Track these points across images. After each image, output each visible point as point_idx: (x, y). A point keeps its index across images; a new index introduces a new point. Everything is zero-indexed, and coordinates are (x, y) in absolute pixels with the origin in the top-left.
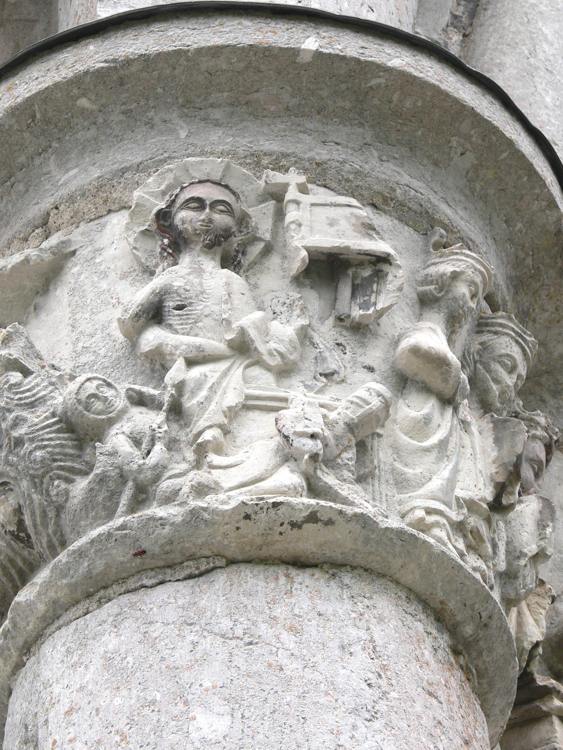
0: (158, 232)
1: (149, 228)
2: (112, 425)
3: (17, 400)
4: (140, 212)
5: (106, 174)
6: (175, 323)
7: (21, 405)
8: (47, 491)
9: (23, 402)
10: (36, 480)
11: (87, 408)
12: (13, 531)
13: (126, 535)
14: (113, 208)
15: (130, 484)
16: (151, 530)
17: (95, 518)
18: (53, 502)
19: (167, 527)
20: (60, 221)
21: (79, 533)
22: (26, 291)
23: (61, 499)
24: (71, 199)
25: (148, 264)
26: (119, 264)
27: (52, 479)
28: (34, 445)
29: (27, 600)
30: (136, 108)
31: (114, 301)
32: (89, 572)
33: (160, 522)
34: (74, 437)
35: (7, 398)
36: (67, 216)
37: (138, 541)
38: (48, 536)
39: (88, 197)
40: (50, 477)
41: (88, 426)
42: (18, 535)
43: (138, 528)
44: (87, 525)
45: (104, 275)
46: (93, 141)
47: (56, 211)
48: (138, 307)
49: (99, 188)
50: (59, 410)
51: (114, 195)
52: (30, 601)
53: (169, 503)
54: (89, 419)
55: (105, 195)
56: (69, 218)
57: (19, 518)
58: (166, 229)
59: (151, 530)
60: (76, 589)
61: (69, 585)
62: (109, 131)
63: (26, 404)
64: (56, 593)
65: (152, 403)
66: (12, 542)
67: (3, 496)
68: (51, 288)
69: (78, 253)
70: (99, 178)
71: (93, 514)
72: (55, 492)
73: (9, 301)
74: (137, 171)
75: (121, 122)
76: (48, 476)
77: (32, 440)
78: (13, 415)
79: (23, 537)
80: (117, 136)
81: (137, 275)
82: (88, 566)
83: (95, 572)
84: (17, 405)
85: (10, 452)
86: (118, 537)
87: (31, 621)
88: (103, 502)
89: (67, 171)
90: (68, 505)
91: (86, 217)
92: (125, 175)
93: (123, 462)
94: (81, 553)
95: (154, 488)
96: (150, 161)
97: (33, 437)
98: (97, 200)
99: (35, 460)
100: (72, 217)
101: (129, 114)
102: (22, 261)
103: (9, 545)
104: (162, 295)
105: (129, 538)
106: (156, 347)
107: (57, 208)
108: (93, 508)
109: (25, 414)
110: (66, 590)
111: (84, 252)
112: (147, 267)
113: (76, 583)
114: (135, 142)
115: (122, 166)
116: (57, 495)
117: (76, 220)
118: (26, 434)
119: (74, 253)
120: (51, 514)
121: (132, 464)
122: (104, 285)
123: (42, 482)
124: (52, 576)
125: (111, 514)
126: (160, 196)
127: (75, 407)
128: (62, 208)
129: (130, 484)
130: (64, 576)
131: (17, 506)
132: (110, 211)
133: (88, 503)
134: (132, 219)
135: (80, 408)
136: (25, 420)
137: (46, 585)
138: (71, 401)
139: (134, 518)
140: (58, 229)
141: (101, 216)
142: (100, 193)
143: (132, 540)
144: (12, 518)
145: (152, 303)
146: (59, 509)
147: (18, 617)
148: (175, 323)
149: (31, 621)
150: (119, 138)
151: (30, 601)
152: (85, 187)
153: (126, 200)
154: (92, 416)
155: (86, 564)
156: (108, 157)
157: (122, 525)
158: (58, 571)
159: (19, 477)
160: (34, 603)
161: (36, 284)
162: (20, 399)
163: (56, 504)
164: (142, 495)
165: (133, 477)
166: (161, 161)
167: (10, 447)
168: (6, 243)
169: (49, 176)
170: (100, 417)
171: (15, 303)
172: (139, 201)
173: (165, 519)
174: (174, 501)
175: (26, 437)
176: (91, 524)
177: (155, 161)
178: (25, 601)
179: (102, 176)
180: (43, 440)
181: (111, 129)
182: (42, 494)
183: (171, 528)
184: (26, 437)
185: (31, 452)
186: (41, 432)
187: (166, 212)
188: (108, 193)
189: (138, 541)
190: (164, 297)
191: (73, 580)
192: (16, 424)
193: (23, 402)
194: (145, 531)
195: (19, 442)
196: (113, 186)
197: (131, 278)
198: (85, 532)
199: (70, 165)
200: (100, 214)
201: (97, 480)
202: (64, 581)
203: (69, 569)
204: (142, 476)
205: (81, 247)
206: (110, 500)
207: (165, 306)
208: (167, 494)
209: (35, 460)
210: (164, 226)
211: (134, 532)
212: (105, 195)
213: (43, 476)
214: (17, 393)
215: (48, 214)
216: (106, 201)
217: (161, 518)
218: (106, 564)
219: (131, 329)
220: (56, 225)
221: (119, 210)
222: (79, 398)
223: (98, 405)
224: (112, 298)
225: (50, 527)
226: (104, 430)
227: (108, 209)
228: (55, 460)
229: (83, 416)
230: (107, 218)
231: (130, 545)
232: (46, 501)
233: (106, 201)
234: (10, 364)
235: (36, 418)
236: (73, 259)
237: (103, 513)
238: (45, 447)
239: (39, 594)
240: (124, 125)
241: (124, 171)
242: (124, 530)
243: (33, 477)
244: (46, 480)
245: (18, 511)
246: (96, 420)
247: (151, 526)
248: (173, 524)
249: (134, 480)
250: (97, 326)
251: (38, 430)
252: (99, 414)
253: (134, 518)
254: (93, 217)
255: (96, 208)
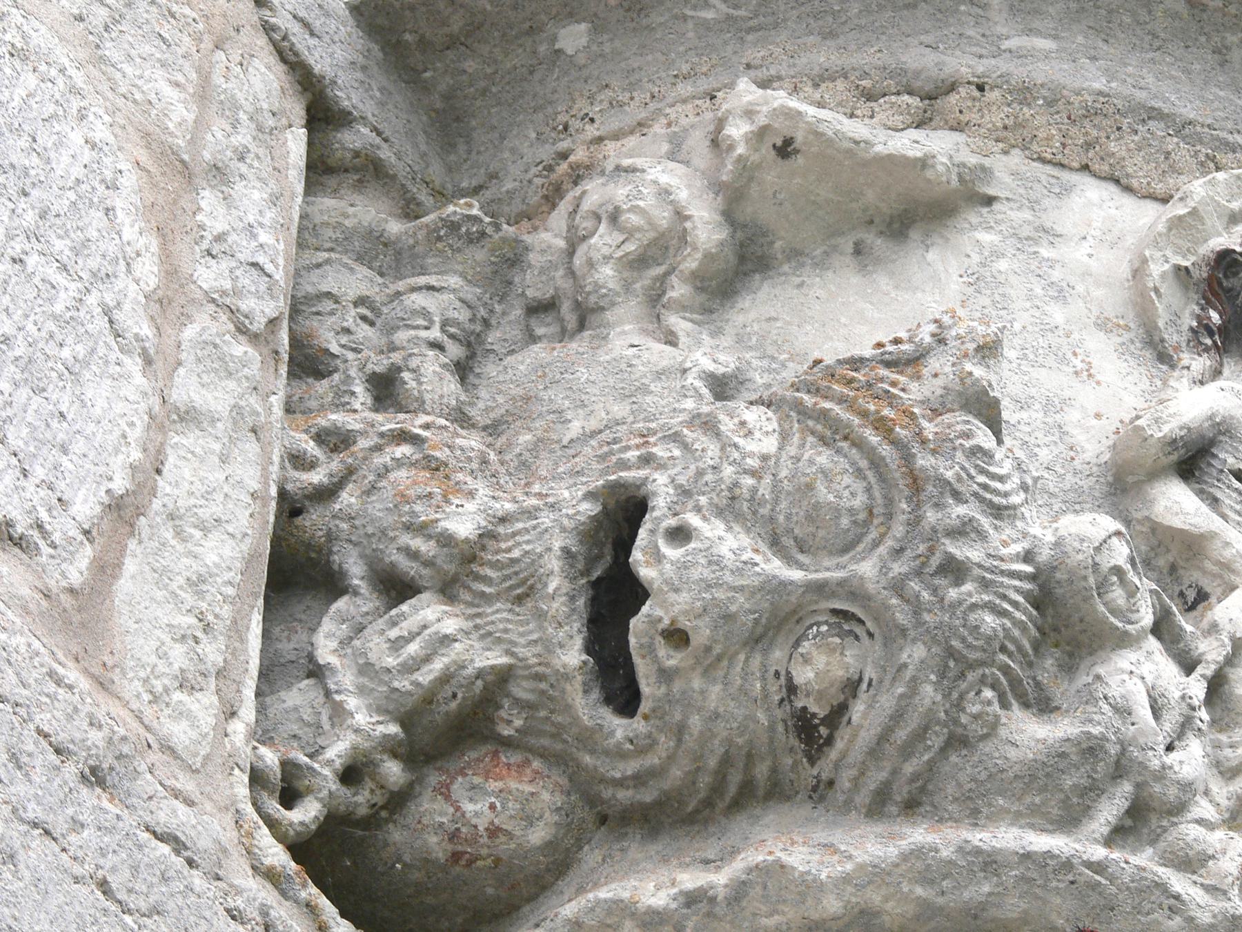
0: (1204, 286)
1: (1191, 268)
2: (1121, 648)
3: (979, 484)
4: (1191, 227)
5: (1117, 96)
6: (1227, 501)
7: (982, 500)
8: (961, 697)
9: (988, 496)
10: (952, 664)
11: (1102, 588)
12: (814, 715)
13: (1096, 886)
14: (1095, 167)
15: (1127, 787)
16: (1147, 906)
17: (1034, 810)
18: (956, 722)
19: (1178, 919)
20: (975, 117)
21: (975, 813)
22: (854, 205)
23: (978, 729)
24: (1024, 93)
25: (1166, 336)
26: (1098, 293)
27: (983, 681)
28: (986, 598)
29: (809, 873)
30: (1215, 10)
31: (1080, 366)
32: (983, 906)
33: (1172, 901)
34: (1039, 622)
35: (963, 468)
36: (997, 118)
37: (1112, 909)
38: (895, 772)
39: (1058, 113)
40: (984, 675)
41: (1081, 621)
42: (816, 726)
43: (1128, 888)
44: (1008, 811)
45: (1061, 294)
46: (1103, 12)
47: (977, 94)
48: (1181, 428)
49: (1091, 113)
50: (1044, 555)
51: (1113, 146)
52: (814, 881)
53: (1185, 871)
54: (1095, 611)
55: (1095, 133)
56: (999, 125)
57: (846, 699)
58: (1220, 292)
59: (1147, 906)
60: (930, 919)
61: (925, 904)
62: (1143, 15)
63: (991, 504)
64: (886, 899)
65: (1172, 642)
66: (780, 728)
67: (838, 640)
68: (915, 234)
69: (996, 206)
70: (1100, 93)
71: (1037, 800)
72: (975, 709)
73: (814, 202)
74: (1178, 133)
75: (1175, 16)
76: (980, 672)
77: (985, 585)
78: (961, 510)
79: (820, 736)
80: (1155, 36)
81: (1132, 342)
82: (990, 894)
83: (994, 912)
84: (975, 495)
85: (918, 573)
86: (1082, 879)
87: (784, 913)
88: (1059, 787)
89: (1030, 31)
90: (987, 747)
91: (1035, 147)
92: (1151, 123)
93: (1134, 738)
94: (989, 862)
95: (1165, 823)
96: (1206, 130)
97: (993, 582)
98: (1074, 131)
99: (977, 627)
100: (1005, 128)
101: (1196, 11)
102: (917, 159)
103: (772, 728)
104: (1220, 432)
105: (1100, 894)
106: (1202, 535)
107: (981, 88)
108: (1043, 789)
109: (985, 522)
110: (910, 909)
111: (1013, 215)
112: (1163, 340)
113: (941, 909)
114: (1187, 72)
115: (1153, 103)
116: (976, 717)
117: (1012, 136)
118: (980, 566)
119: (989, 201)
120: (936, 741)
121: (1150, 753)
122: (1057, 314)
123: (962, 676)
124: (897, 865)
125: (1070, 818)
126: (1226, 219)
127: (1083, 572)
128: (993, 95)
129: (1127, 787)
130: (926, 878)
131: (856, 677)
132: (1085, 168)
133: (1041, 774)
134: (1170, 229)
135: (1092, 581)
136: (982, 536)
137: (875, 875)
138: (1080, 557)
139: (1127, 862)
140: (958, 128)
141: (1063, 166)
142: (1086, 123)
143: (1102, 902)
144: (833, 690)
145: (1203, 437)
146: (958, 741)
147: (758, 889)
148: (1227, 501)
149: (784, 913)
150: (1157, 43)
151: (814, 881)
152: (1065, 92)
153: (1130, 170)
154: (1102, 608)
155: (986, 889)
156: (1126, 65)
157: (1099, 863)
158: (919, 865)
159: (912, 633)
160: (821, 887)
161: (882, 205)
162: (985, 487)
163: (960, 730)
164: (1138, 822)
165: (1139, 779)
166: (1227, 144)
167: (923, 564)
168: (816, 70)
169: (980, 11)
170: (1112, 619)
171: (820, 213)
172: (1200, 209)
173: (1183, 902)
174: (1194, 872)
175: (977, 571)
176: (1018, 815)
177: (1218, 139)
178: (802, 874)
179: (1108, 95)
180: (1004, 597)
181: (1150, 12)
182: (946, 696)
183: (1184, 924)
184: (977, 571)
185: (974, 607)
186: (1006, 580)
187: (1236, 260)
188: (1103, 134)
189: (1112, 909)
190: (1221, 438)
191: (940, 900)
192: (964, 530)
193: (988, 496)
194: (1137, 900)
195: (955, 570)
196: (1119, 129)
197: (1119, 340)
198: (995, 818)
199: (1037, 24)
200: (1066, 162)
201: (1084, 746)
202: (919, 891)
203: (945, 877)
204: (1157, 788)
205: (1008, 199)
206: (1081, 796)
207: (1215, 456)
208: (1191, 853)
209: (977, 627)
210: (1220, 284)
211: (1113, 889)
212: (1095, 133)
213: (972, 666)
214: (983, 471)
215: (952, 88)
216: (1088, 146)
217: (1177, 897)
218: (1025, 912)
219: (1150, 461)
220: (962, 117)
221: (1145, 197)
222: (1097, 559)
223: (1118, 595)
224: (1075, 354)
225: (915, 761)
226: (1101, 647)
227: (1085, 161)
228: (1003, 649)
229: (1087, 599)
230: (1075, 178)
231: (1094, 907)
232: (946, 712)
233: (1088, 146)
234: (978, 400)
235: (1006, 544)
236: (985, 210)
237: (1055, 811)
238: (1002, 613)
239: (846, 879)
240: (1176, 24)
241: (1154, 114)
242: (1096, 873)
243: (951, 653)
244: (972, 676)
245: (852, 686)
246: (1104, 620)
247: (1153, 898)
248: (1191, 920)
249: (1138, 786)
250: (1033, 392)
251: (1002, 572)
252: (1112, 612)
253: (1127, 862)
254: (1049, 156)
255: (1064, 145)
